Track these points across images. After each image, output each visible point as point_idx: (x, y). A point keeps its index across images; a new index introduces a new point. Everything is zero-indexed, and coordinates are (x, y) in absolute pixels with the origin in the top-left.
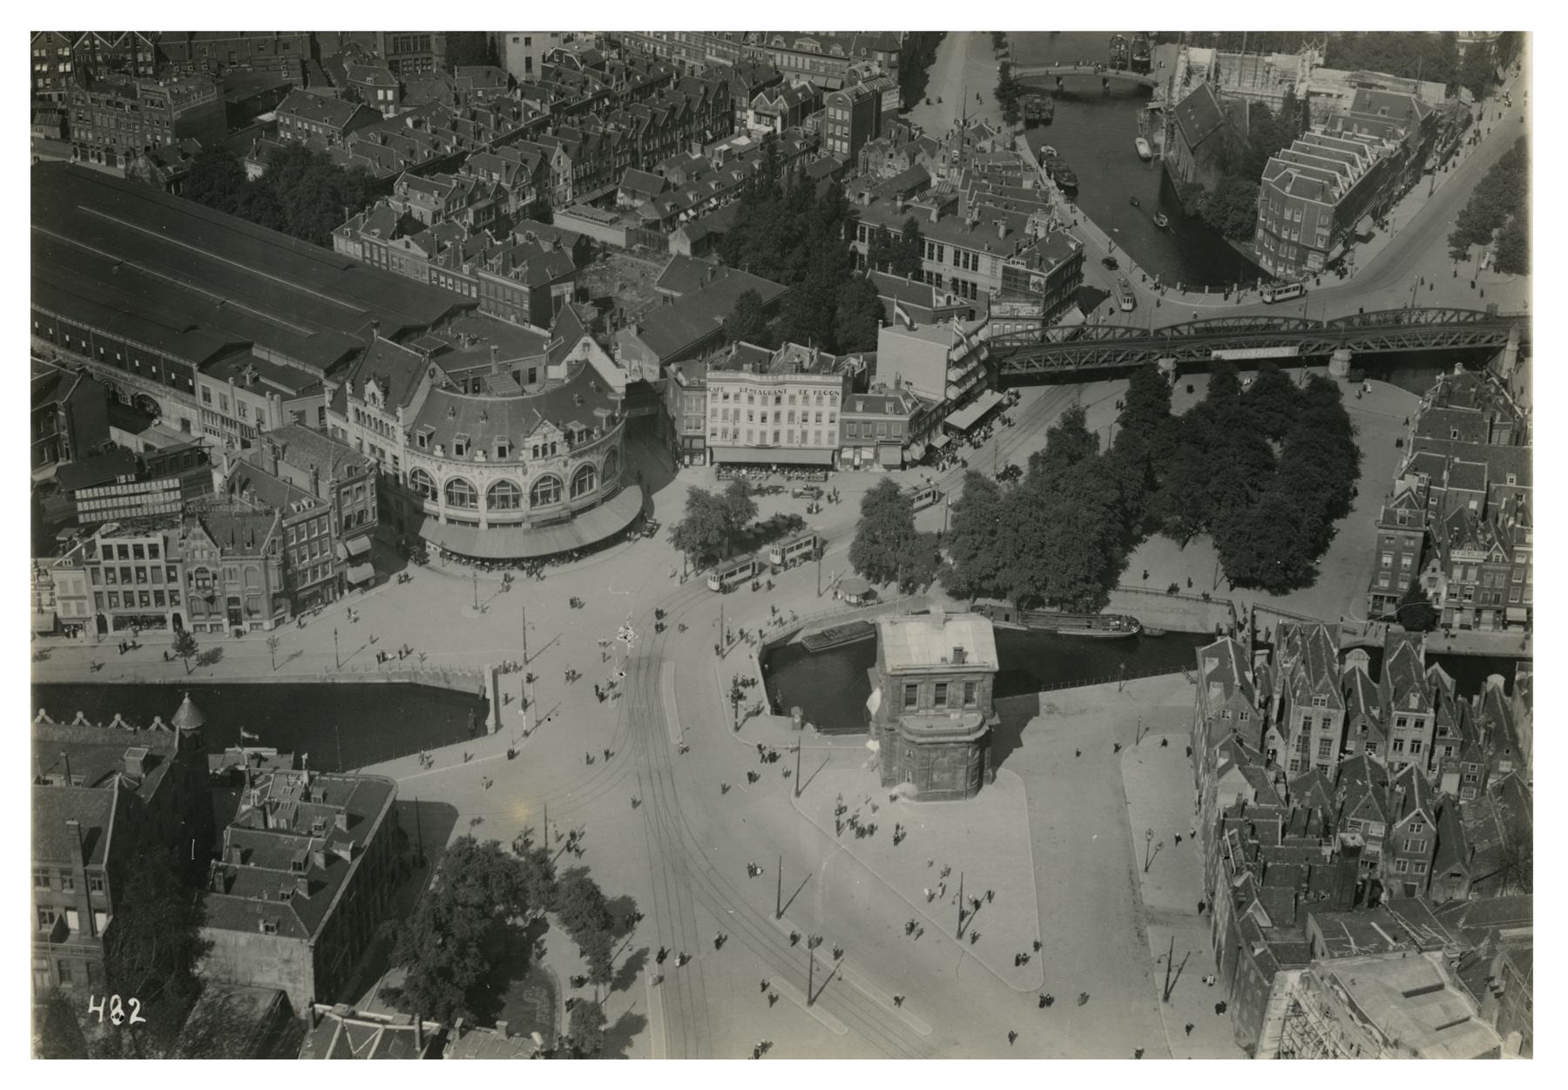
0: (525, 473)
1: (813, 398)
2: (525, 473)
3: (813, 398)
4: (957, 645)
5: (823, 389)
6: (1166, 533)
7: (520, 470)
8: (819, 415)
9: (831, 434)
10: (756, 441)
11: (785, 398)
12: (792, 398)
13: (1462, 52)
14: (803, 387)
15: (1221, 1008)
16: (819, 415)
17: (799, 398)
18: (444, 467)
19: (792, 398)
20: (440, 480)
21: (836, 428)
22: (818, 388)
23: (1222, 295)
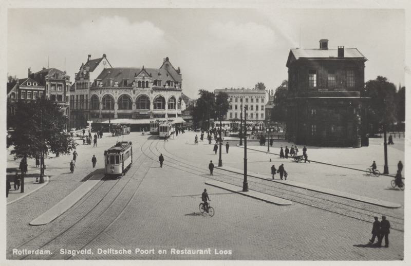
0: (134, 93)
1: (255, 100)
2: (134, 93)
3: (255, 100)
4: (324, 38)
5: (258, 95)
6: (185, 110)
7: (132, 91)
8: (252, 106)
9: (262, 115)
10: (234, 117)
11: (244, 100)
12: (247, 100)
13: (216, 98)
14: (251, 95)
15: (324, 45)
16: (252, 106)
17: (249, 100)
18: (102, 91)
19: (247, 100)
20: (152, 98)
21: (264, 112)
22: (256, 95)
23: (347, 55)
